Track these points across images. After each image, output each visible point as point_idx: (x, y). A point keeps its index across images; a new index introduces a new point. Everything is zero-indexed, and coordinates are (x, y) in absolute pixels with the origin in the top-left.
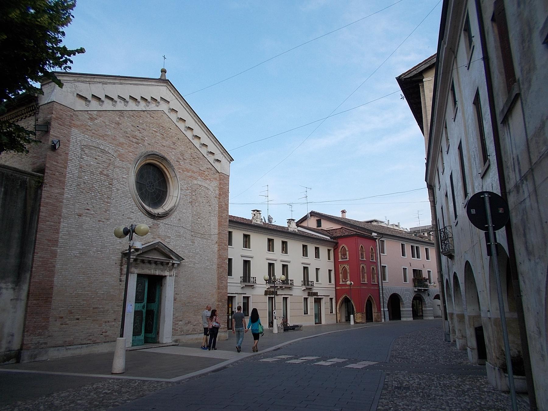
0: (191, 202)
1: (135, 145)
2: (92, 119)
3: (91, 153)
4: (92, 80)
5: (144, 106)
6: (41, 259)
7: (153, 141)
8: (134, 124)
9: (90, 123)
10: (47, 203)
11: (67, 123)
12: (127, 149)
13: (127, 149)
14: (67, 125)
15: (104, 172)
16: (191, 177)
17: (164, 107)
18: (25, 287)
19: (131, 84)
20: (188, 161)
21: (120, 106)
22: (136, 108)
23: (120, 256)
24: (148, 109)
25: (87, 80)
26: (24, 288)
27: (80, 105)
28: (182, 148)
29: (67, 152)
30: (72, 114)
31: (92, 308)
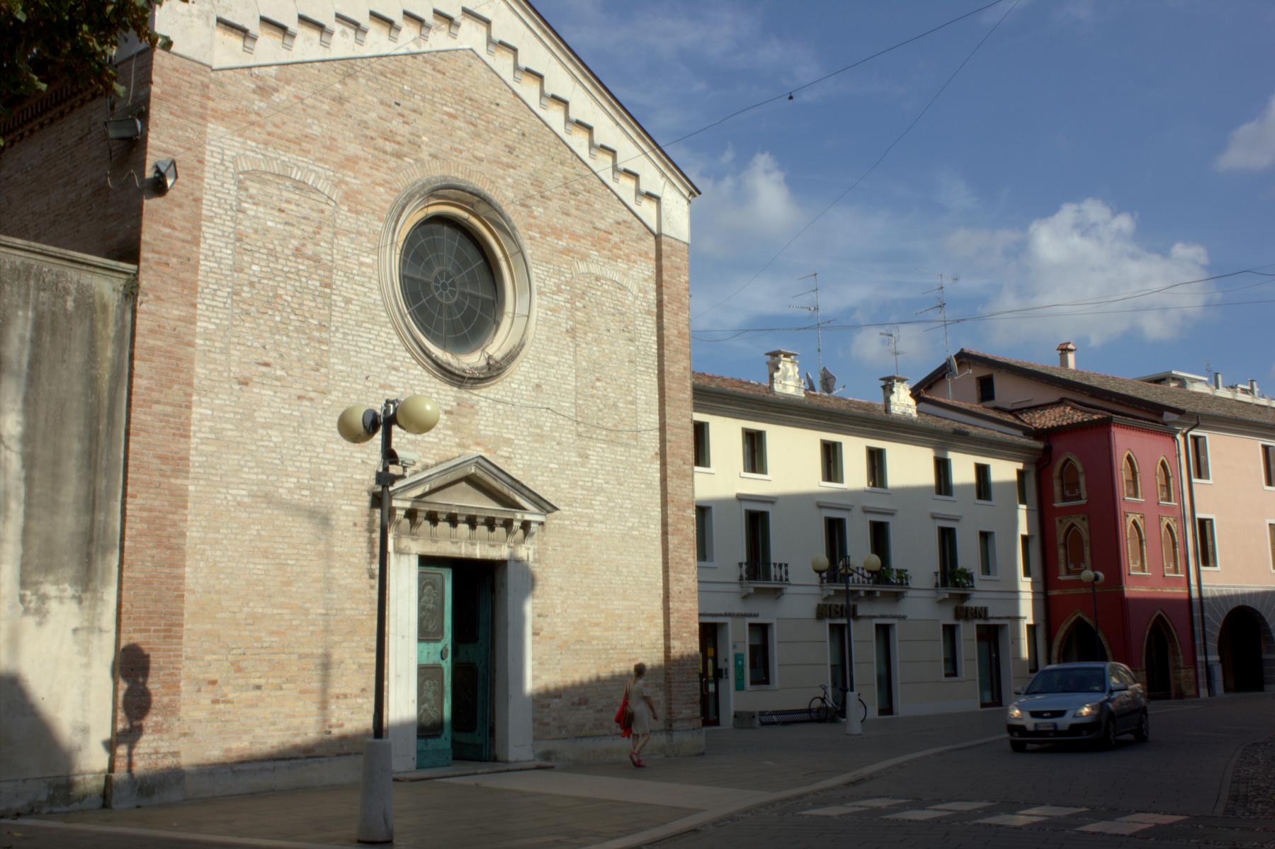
0: (572, 332)
1: (393, 162)
2: (264, 91)
3: (266, 195)
6: (145, 514)
7: (446, 145)
9: (259, 104)
12: (368, 175)
13: (368, 175)
14: (196, 115)
16: (567, 251)
24: (425, 47)
26: (105, 597)
29: (197, 194)
31: (295, 657)
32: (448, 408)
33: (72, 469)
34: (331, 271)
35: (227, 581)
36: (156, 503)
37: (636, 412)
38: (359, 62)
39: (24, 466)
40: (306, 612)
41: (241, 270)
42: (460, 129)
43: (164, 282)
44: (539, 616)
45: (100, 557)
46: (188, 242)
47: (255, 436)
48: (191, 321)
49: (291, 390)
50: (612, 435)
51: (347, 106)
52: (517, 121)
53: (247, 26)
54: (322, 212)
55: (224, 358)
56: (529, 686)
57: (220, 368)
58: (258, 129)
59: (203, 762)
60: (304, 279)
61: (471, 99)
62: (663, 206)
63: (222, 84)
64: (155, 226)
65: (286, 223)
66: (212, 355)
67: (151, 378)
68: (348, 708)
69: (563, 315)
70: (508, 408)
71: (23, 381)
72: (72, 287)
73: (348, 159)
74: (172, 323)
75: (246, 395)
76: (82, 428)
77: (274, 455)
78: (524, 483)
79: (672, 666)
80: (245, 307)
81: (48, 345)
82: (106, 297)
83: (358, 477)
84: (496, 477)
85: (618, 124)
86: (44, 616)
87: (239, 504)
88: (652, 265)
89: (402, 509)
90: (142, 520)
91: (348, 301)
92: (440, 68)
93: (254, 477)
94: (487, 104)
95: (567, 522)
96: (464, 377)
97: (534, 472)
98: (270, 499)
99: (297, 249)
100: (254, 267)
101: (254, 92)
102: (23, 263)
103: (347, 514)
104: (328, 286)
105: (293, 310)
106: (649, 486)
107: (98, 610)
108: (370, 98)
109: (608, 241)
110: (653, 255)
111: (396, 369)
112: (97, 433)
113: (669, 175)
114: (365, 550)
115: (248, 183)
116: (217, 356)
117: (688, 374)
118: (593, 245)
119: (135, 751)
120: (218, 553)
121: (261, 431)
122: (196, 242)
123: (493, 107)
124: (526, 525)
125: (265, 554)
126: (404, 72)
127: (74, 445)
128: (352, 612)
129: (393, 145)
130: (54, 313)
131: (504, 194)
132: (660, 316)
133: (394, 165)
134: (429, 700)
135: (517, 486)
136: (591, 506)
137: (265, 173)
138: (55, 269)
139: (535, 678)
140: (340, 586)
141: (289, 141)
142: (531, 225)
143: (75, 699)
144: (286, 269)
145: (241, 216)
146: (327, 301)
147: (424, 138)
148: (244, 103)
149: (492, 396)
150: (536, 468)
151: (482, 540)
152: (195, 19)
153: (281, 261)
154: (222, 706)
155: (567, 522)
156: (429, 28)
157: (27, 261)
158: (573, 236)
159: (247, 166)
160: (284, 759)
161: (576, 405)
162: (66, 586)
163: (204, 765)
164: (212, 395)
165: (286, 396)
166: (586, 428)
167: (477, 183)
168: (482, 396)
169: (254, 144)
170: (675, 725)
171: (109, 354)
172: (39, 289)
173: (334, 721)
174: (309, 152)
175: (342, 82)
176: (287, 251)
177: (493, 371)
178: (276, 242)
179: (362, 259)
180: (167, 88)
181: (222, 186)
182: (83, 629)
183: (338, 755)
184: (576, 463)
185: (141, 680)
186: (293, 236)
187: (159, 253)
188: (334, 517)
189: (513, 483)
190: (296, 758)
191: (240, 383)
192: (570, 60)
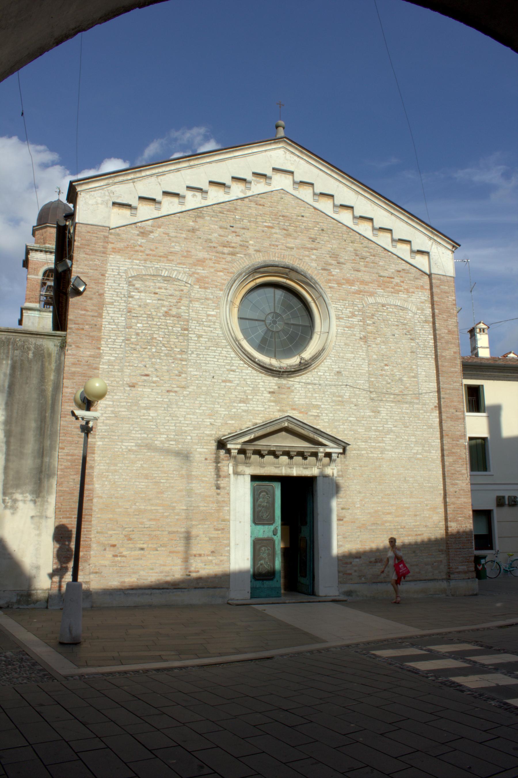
0: (365, 339)
1: (229, 258)
2: (144, 234)
3: (146, 286)
4: (138, 175)
5: (242, 191)
6: (69, 458)
7: (266, 244)
8: (224, 224)
9: (141, 241)
10: (74, 373)
11: (99, 250)
12: (212, 267)
13: (212, 267)
14: (100, 252)
15: (171, 312)
16: (359, 292)
17: (281, 182)
18: (52, 499)
19: (210, 162)
20: (349, 266)
21: (193, 201)
22: (226, 198)
23: (213, 446)
24: (249, 193)
25: (129, 177)
26: (49, 500)
27: (118, 218)
28: (334, 244)
29: (101, 291)
30: (106, 234)
31: (166, 533)
32: (272, 390)
33: (31, 437)
34: (188, 322)
35: (122, 492)
36: (76, 452)
37: (417, 382)
38: (205, 209)
39: (5, 436)
40: (174, 508)
41: (131, 327)
42: (276, 233)
43: (80, 338)
44: (343, 509)
45: (46, 480)
46: (95, 316)
47: (139, 413)
48: (99, 356)
49: (162, 388)
50: (399, 398)
51: (198, 233)
52: (318, 223)
53: (130, 203)
54: (182, 290)
55: (120, 374)
56: (335, 551)
57: (118, 380)
58: (140, 254)
59: (107, 588)
60: (170, 328)
61: (283, 216)
62: (431, 257)
63: (118, 235)
64: (76, 311)
65: (159, 300)
66: (113, 373)
67: (74, 388)
68: (202, 562)
69: (357, 330)
70: (316, 387)
71: (5, 395)
72: (32, 347)
73: (198, 261)
74: (86, 359)
75: (134, 392)
76: (36, 416)
77: (151, 423)
78: (322, 430)
79: (450, 542)
80: (133, 346)
81: (18, 376)
82: (50, 349)
83: (208, 432)
84: (303, 428)
85: (392, 214)
86: (15, 510)
87: (129, 450)
88: (427, 293)
89: (235, 449)
90: (68, 460)
91: (199, 336)
92: (261, 203)
93: (139, 436)
94: (295, 217)
95: (363, 452)
96: (280, 372)
97: (337, 424)
98: (150, 447)
99: (166, 312)
100: (139, 325)
101: (138, 235)
102: (6, 338)
103: (200, 453)
104: (186, 329)
105: (164, 345)
106: (430, 427)
107: (45, 507)
108: (212, 226)
109: (392, 283)
110: (428, 287)
111: (234, 371)
112: (45, 417)
113: (435, 238)
114: (213, 473)
115: (135, 282)
116: (116, 373)
117: (458, 356)
118: (379, 286)
119: (63, 580)
120: (116, 477)
121: (143, 411)
122: (100, 316)
123: (300, 218)
124: (328, 455)
125: (146, 477)
126: (236, 209)
127: (32, 424)
128: (205, 508)
129: (229, 249)
130: (22, 360)
131: (309, 265)
132: (434, 323)
133: (230, 259)
134: (265, 559)
135: (318, 432)
136: (383, 441)
137: (145, 275)
138: (23, 339)
139: (339, 546)
140: (196, 494)
141: (160, 257)
142: (330, 280)
143: (36, 554)
144: (158, 324)
145: (130, 299)
146: (186, 338)
147: (251, 242)
148: (132, 242)
149: (304, 381)
150: (339, 421)
151: (298, 465)
152: (100, 205)
153: (155, 320)
154: (119, 558)
155: (363, 452)
156: (250, 183)
157: (8, 337)
158: (363, 282)
159: (134, 274)
160: (159, 589)
161: (369, 382)
162: (27, 495)
163: (108, 590)
164: (113, 394)
165: (160, 391)
166: (377, 395)
167: (289, 261)
168: (296, 382)
169: (138, 262)
170: (452, 576)
171: (52, 377)
172: (14, 349)
173: (192, 569)
174: (173, 260)
175: (195, 221)
176: (159, 314)
177: (304, 367)
178: (153, 310)
179: (209, 313)
180: (84, 242)
181: (119, 285)
182: (37, 516)
183: (195, 588)
184: (370, 417)
185: (67, 543)
186: (163, 306)
187: (78, 324)
188: (192, 455)
189: (315, 431)
190: (168, 589)
191: (130, 386)
192: (353, 183)
